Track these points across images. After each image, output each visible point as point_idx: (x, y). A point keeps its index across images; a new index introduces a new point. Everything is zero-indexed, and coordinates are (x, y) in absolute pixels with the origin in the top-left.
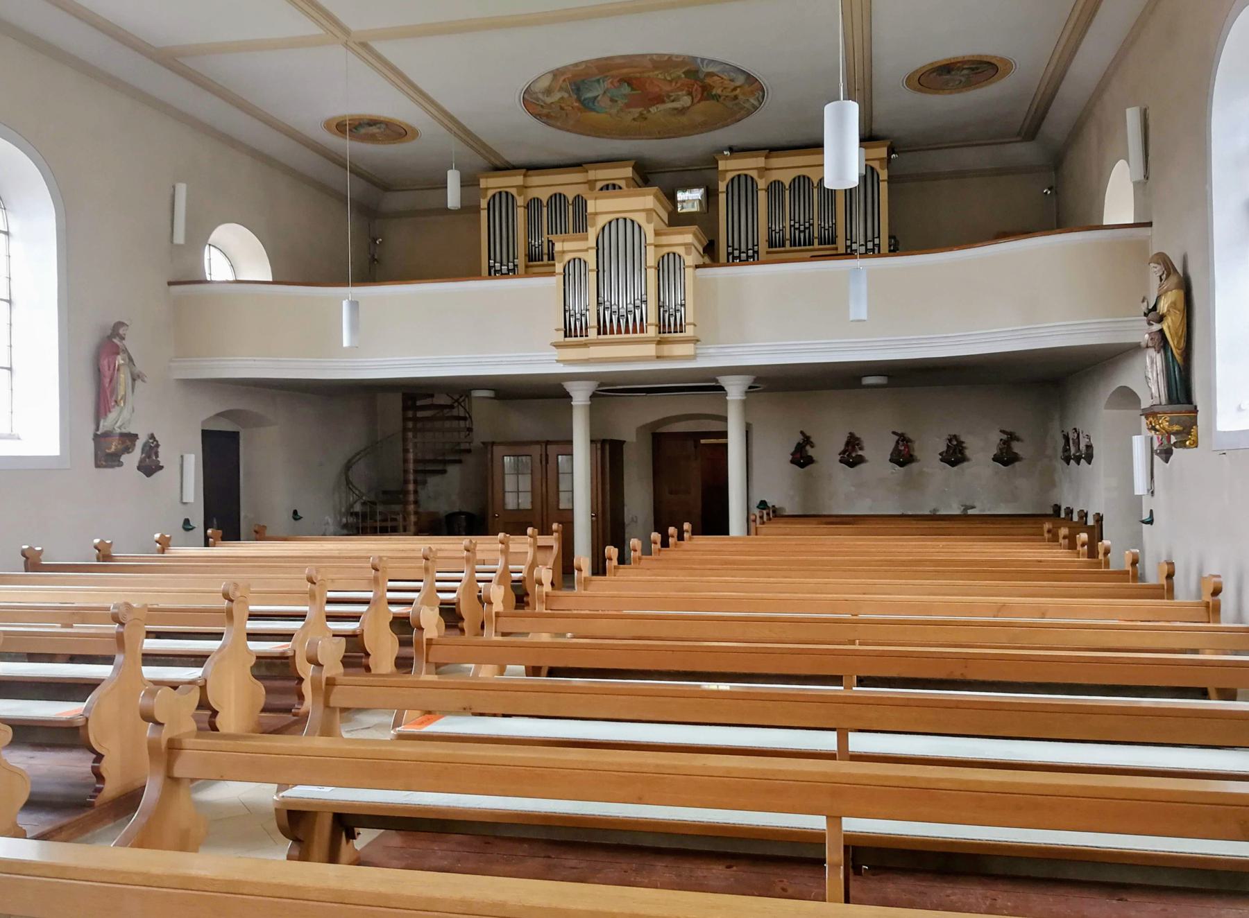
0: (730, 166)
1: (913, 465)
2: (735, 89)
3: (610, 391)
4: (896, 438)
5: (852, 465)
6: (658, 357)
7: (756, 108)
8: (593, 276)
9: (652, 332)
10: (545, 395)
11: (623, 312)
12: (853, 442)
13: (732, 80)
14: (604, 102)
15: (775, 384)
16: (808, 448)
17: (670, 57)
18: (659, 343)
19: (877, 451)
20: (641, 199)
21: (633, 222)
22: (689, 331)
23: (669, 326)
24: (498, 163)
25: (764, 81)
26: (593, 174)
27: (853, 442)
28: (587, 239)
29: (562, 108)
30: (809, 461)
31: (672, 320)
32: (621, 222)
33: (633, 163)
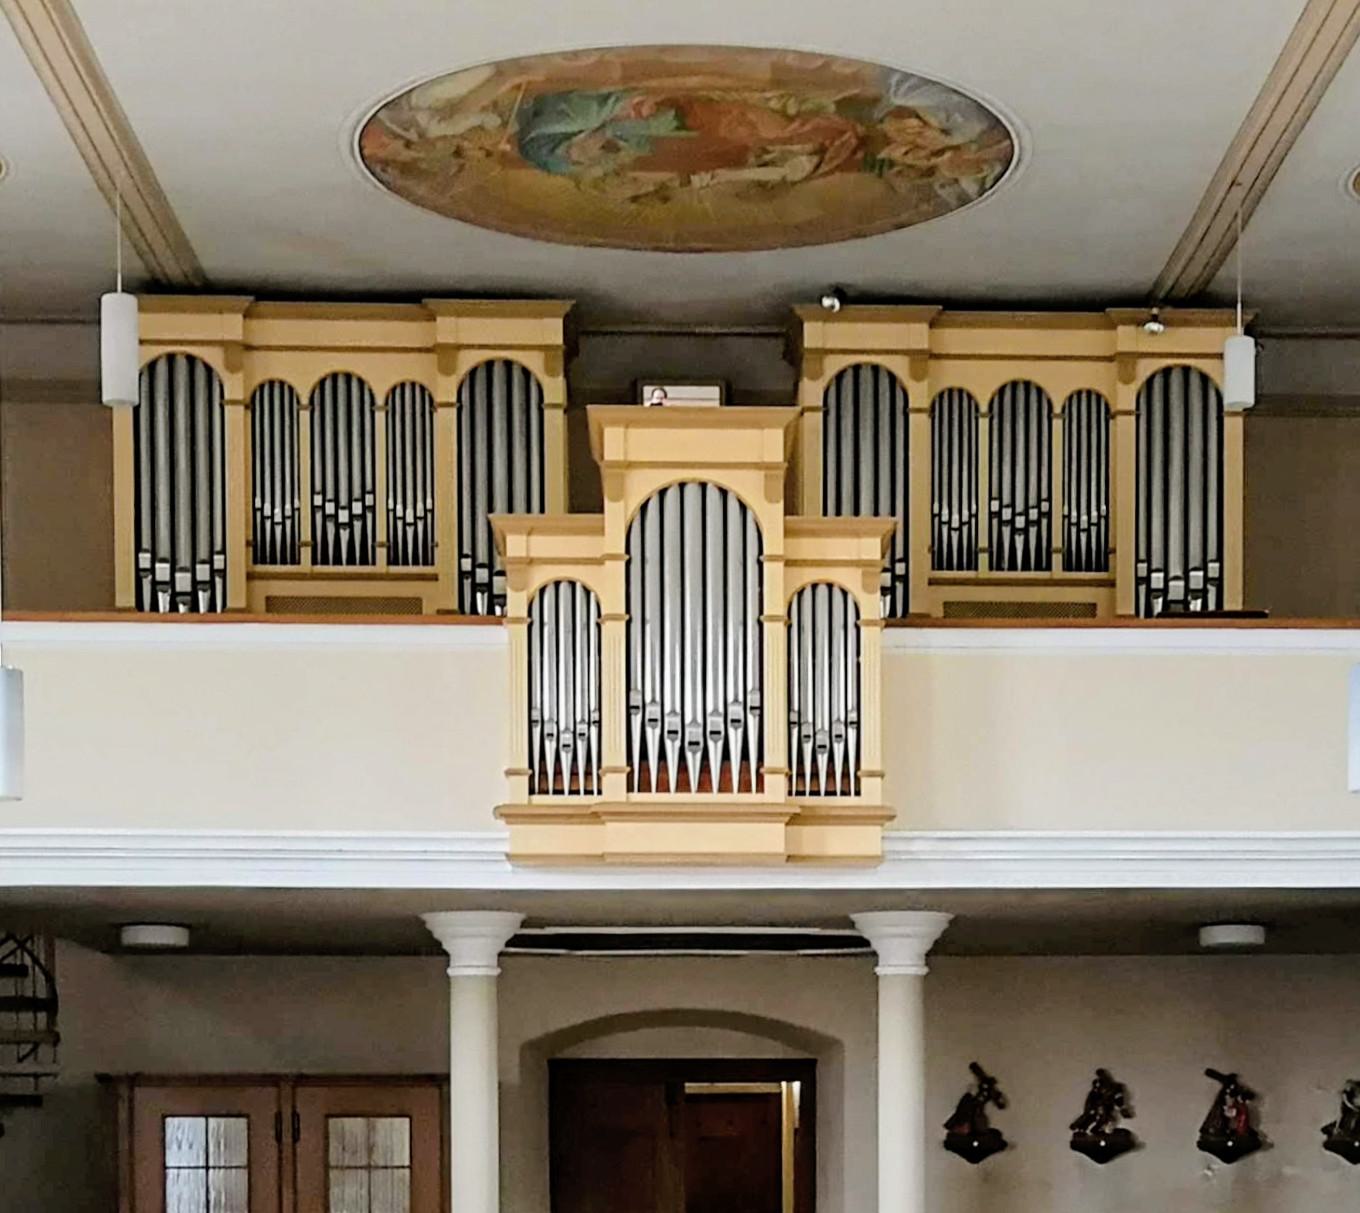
0: (835, 338)
1: (1259, 1156)
2: (940, 152)
3: (546, 936)
4: (1217, 1086)
5: (1102, 1156)
6: (790, 858)
7: (964, 200)
8: (614, 632)
9: (776, 788)
10: (382, 943)
11: (694, 733)
12: (1107, 1096)
13: (945, 132)
14: (586, 149)
15: (995, 945)
16: (990, 1109)
17: (829, 61)
18: (794, 820)
19: (1168, 1115)
20: (750, 434)
21: (724, 493)
22: (872, 792)
23: (825, 774)
24: (173, 269)
25: (1023, 141)
26: (451, 327)
27: (1107, 1096)
28: (600, 531)
29: (458, 153)
30: (995, 1143)
31: (823, 760)
32: (692, 494)
33: (567, 306)
